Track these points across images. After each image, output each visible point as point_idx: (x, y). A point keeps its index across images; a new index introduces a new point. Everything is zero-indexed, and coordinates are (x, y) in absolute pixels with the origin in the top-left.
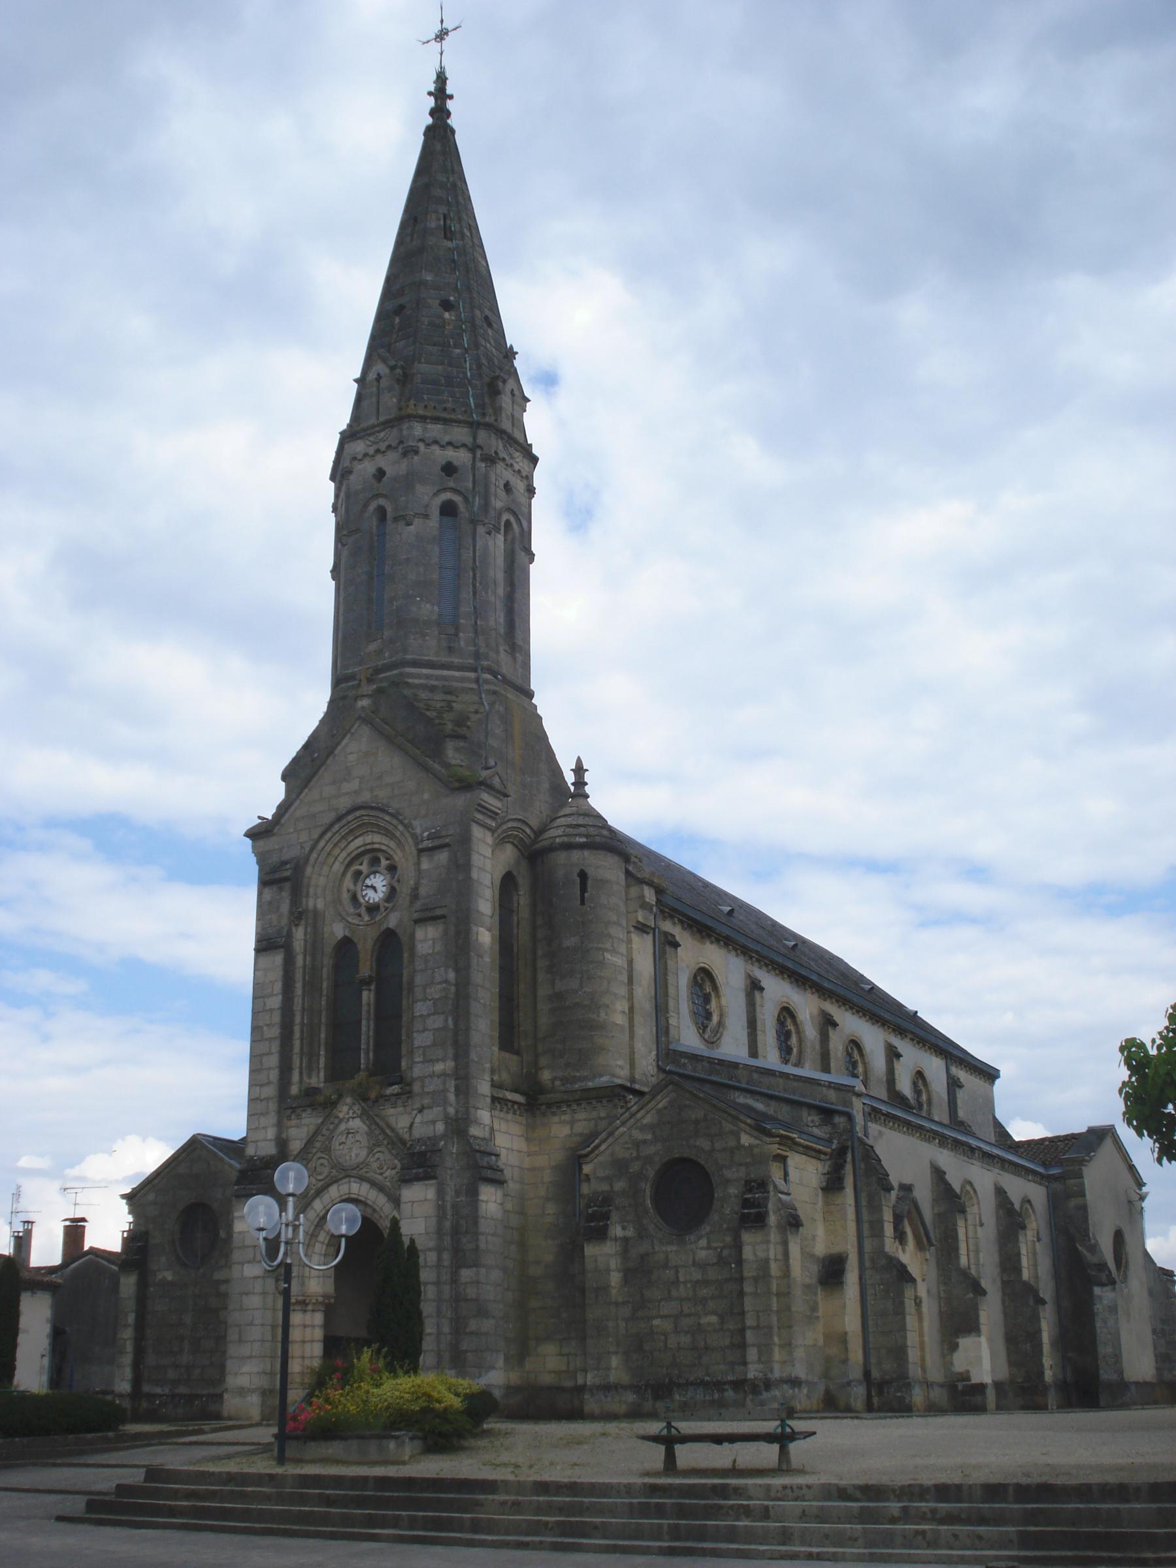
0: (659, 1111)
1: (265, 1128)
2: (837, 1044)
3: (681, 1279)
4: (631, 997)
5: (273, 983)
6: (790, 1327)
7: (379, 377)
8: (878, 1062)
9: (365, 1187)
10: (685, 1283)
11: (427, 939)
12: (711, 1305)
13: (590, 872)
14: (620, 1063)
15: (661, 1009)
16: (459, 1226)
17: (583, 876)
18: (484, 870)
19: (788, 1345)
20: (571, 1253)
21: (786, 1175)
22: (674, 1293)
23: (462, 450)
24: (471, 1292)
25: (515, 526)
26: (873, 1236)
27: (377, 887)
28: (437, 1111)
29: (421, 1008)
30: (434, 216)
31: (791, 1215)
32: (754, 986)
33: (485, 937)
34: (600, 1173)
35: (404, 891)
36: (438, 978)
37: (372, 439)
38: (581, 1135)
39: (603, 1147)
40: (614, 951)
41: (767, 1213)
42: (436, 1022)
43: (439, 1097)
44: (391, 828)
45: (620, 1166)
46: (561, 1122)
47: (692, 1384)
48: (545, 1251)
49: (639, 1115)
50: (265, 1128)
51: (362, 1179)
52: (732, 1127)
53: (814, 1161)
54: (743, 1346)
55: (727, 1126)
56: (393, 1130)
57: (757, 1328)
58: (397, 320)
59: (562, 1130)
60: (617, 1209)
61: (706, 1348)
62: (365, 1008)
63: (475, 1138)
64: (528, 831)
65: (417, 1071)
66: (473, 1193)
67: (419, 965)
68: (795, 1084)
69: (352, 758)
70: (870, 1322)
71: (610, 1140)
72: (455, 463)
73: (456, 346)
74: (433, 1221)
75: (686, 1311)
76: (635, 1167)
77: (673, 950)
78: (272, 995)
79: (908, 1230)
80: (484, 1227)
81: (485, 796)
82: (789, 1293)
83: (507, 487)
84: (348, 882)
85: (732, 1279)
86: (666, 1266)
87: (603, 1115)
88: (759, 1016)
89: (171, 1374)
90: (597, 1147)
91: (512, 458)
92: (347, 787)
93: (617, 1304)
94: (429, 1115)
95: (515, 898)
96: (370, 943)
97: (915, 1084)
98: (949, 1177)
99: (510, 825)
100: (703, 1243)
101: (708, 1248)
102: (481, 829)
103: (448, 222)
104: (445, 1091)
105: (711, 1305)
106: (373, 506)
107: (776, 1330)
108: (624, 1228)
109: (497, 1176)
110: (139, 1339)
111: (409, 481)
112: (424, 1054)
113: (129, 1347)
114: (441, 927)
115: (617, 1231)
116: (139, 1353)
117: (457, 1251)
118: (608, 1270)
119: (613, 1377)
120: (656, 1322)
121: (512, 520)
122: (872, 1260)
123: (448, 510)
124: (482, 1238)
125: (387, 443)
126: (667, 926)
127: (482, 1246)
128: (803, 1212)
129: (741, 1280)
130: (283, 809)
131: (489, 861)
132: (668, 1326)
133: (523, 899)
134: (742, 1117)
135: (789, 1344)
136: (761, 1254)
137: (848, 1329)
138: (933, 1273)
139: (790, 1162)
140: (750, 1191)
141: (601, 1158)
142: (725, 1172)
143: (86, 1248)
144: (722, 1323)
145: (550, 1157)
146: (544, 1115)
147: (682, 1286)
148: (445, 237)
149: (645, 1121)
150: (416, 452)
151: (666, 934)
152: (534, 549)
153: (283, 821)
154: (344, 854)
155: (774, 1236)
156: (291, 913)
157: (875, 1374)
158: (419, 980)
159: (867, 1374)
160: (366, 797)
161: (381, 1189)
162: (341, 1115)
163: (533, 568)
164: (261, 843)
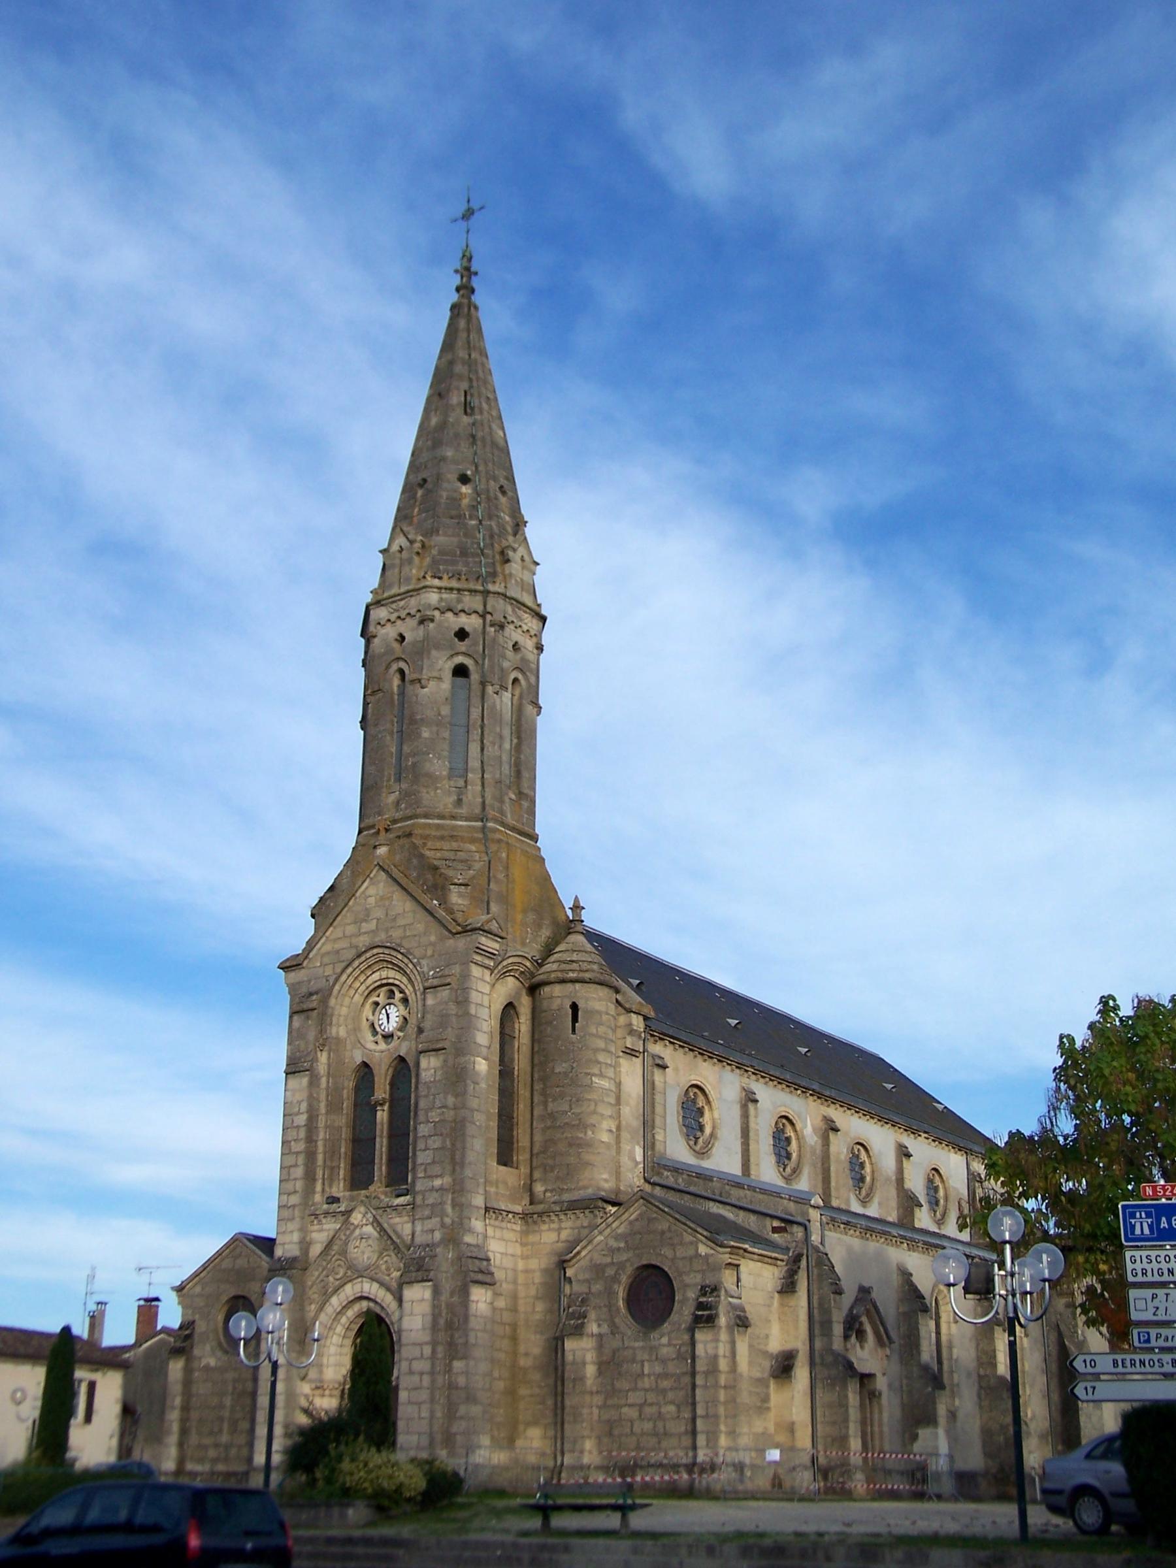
0: (631, 1223)
1: (292, 1232)
2: (839, 1147)
3: (646, 1372)
4: (618, 1116)
5: (300, 1103)
6: (735, 1416)
7: (401, 550)
8: (888, 1162)
9: (375, 1285)
10: (649, 1375)
11: (430, 1066)
12: (670, 1395)
13: (581, 1005)
14: (605, 1176)
15: (648, 1124)
16: (451, 1325)
17: (575, 1007)
18: (482, 1005)
19: (732, 1433)
20: (556, 1346)
21: (738, 1280)
22: (640, 1385)
23: (474, 616)
24: (461, 1381)
25: (523, 682)
26: (823, 1335)
27: (391, 1019)
28: (435, 1221)
29: (423, 1130)
30: (456, 392)
31: (739, 1317)
32: (750, 1099)
33: (483, 1066)
34: (581, 1277)
35: (413, 1021)
36: (438, 1104)
37: (394, 606)
38: (567, 1241)
39: (583, 1254)
40: (601, 1075)
41: (717, 1315)
42: (435, 1143)
43: (436, 1210)
44: (402, 965)
45: (598, 1270)
46: (549, 1230)
47: (652, 1466)
48: (533, 1345)
49: (614, 1225)
50: (292, 1232)
51: (373, 1279)
52: (692, 1238)
53: (771, 1268)
54: (694, 1433)
55: (688, 1238)
56: (399, 1237)
57: (706, 1416)
58: (420, 493)
59: (551, 1236)
60: (594, 1308)
61: (665, 1434)
62: (378, 1127)
63: (469, 1245)
64: (528, 964)
65: (419, 1186)
66: (464, 1292)
67: (423, 1091)
68: (761, 1196)
69: (372, 900)
70: (818, 1413)
71: (589, 1248)
72: (467, 629)
73: (471, 518)
74: (429, 1318)
75: (649, 1401)
76: (610, 1272)
77: (661, 1071)
78: (299, 1113)
79: (868, 1328)
80: (473, 1323)
81: (483, 940)
82: (734, 1387)
83: (516, 647)
84: (367, 1010)
85: (690, 1374)
86: (633, 1361)
87: (585, 1224)
88: (752, 1125)
89: (212, 1453)
90: (578, 1253)
91: (521, 620)
92: (365, 927)
93: (591, 1393)
94: (429, 1224)
95: (517, 1026)
96: (384, 1067)
97: (930, 1181)
98: (914, 1279)
99: (510, 960)
100: (665, 1340)
101: (669, 1345)
102: (480, 969)
103: (468, 398)
104: (442, 1203)
105: (670, 1395)
106: (395, 667)
107: (722, 1419)
108: (599, 1326)
109: (488, 1279)
110: (184, 1421)
111: (422, 650)
112: (425, 1170)
113: (175, 1427)
114: (442, 1058)
115: (593, 1328)
116: (184, 1432)
117: (451, 1345)
118: (584, 1364)
119: (586, 1460)
120: (625, 1410)
121: (520, 677)
122: (822, 1356)
123: (460, 671)
124: (472, 1335)
125: (407, 611)
126: (657, 1048)
127: (472, 1340)
128: (751, 1313)
129: (693, 1374)
130: (311, 944)
131: (489, 994)
132: (633, 1413)
133: (523, 1025)
134: (699, 1229)
135: (734, 1432)
136: (711, 1351)
137: (795, 1418)
138: (895, 1367)
139: (742, 1268)
140: (704, 1295)
141: (582, 1263)
142: (685, 1278)
143: (159, 1327)
144: (679, 1411)
145: (539, 1264)
146: (535, 1222)
147: (646, 1379)
148: (466, 413)
149: (619, 1231)
150: (432, 620)
151: (654, 1056)
152: (541, 702)
153: (311, 955)
154: (363, 987)
155: (724, 1336)
156: (317, 1040)
157: (822, 1460)
158: (422, 1104)
159: (813, 1460)
160: (381, 937)
161: (388, 1289)
162: (356, 1223)
163: (540, 720)
164: (292, 975)
